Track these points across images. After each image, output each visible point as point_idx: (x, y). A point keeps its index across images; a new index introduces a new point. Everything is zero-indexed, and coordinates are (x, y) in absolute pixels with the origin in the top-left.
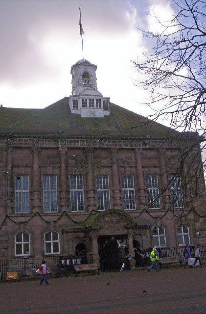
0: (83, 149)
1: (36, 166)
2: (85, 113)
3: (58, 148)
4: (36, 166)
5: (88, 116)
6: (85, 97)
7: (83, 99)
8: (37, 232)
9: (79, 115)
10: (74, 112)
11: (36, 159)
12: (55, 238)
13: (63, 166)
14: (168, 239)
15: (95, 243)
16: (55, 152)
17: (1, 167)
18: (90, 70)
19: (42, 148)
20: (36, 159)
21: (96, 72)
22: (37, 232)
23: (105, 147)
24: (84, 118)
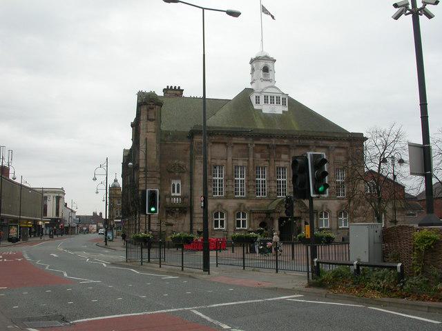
0: (268, 145)
1: (230, 159)
2: (267, 109)
3: (247, 144)
4: (230, 159)
5: (227, 126)
6: (266, 94)
7: (265, 96)
8: (231, 211)
9: (261, 110)
10: (256, 107)
11: (230, 153)
12: (244, 217)
13: (251, 159)
14: (331, 222)
15: (276, 223)
16: (244, 147)
17: (440, 281)
18: (269, 64)
19: (235, 144)
20: (230, 153)
21: (231, 96)
22: (231, 211)
23: (285, 144)
24: (265, 114)
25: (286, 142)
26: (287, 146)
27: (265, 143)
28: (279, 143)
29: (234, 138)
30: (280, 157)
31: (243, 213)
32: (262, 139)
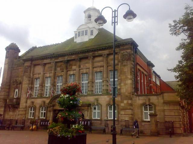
8: (38, 106)
23: (73, 58)
25: (73, 57)
26: (74, 60)
28: (69, 59)
29: (45, 60)
30: (71, 68)
31: (45, 108)
32: (60, 58)
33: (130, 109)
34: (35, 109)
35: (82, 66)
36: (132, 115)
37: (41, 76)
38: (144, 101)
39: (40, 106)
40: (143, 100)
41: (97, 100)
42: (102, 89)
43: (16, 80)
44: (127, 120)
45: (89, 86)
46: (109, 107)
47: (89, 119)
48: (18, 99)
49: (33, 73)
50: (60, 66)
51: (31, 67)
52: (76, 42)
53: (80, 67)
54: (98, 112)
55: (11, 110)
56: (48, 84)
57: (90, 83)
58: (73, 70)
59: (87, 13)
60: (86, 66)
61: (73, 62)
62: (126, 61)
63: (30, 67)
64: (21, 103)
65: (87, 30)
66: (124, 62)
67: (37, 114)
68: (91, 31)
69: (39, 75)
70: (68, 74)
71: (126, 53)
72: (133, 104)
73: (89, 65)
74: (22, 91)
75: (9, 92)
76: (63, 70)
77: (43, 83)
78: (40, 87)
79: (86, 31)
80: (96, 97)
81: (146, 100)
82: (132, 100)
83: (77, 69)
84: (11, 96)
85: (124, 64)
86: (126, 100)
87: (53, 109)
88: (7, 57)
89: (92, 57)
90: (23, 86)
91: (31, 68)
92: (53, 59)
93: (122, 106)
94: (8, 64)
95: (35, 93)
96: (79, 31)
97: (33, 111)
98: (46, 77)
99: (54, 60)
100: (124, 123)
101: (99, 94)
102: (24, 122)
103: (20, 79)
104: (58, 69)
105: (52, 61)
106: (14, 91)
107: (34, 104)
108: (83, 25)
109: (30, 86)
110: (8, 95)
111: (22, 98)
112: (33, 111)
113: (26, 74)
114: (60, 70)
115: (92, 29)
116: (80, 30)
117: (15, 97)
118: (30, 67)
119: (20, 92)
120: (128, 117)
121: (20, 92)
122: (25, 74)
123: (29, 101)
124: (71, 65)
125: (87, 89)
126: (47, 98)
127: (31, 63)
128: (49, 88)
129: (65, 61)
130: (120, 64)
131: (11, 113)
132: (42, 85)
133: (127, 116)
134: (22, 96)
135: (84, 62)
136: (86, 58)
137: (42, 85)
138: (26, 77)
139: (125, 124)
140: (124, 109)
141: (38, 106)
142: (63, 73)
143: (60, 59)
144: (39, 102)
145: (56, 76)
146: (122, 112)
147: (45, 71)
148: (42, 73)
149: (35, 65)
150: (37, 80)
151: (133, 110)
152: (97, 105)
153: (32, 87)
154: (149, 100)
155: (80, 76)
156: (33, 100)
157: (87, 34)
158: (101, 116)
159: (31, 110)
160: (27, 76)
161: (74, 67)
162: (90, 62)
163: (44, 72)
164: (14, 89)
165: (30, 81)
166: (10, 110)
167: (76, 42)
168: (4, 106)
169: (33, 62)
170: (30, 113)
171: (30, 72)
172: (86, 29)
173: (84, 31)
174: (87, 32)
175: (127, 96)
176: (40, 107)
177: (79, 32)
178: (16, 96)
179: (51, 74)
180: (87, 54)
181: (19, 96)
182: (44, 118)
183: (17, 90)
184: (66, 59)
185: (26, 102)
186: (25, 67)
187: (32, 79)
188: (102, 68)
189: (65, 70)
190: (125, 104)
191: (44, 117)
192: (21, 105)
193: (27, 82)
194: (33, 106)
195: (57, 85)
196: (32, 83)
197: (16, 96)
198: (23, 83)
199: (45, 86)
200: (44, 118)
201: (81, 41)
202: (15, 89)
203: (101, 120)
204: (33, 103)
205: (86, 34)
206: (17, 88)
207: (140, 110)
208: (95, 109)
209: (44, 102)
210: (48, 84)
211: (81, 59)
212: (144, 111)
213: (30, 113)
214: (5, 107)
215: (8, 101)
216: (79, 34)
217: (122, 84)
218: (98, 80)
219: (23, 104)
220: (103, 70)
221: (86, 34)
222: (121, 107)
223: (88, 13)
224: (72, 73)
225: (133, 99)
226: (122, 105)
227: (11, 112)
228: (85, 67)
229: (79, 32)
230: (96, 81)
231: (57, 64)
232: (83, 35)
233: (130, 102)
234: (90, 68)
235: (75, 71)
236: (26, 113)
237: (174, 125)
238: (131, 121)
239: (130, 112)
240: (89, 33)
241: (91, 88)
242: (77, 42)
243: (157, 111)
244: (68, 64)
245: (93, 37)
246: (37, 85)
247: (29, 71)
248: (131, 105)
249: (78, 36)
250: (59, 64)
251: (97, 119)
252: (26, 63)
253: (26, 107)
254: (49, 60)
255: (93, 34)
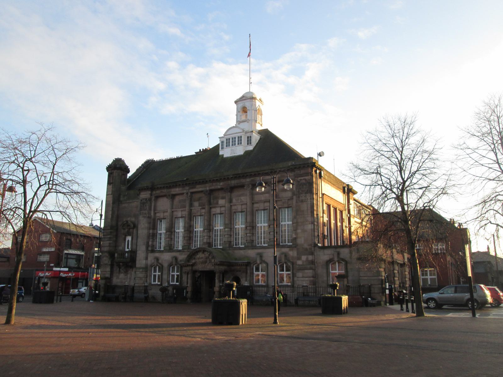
8: (166, 265)
27: (200, 189)
28: (213, 188)
30: (217, 203)
32: (198, 186)
33: (311, 269)
34: (161, 269)
35: (234, 201)
36: (313, 277)
37: (167, 214)
38: (331, 257)
39: (170, 265)
40: (330, 255)
41: (261, 255)
42: (223, 241)
43: (127, 221)
44: (305, 285)
45: (204, 236)
46: (172, 268)
47: (249, 285)
48: (133, 253)
49: (155, 210)
50: (199, 199)
51: (151, 200)
52: (223, 155)
53: (231, 201)
54: (158, 275)
55: (121, 270)
56: (180, 229)
57: (248, 228)
58: (221, 207)
59: (241, 104)
60: (241, 199)
61: (221, 194)
62: (304, 195)
63: (150, 200)
64: (138, 259)
65: (241, 137)
66: (302, 195)
67: (165, 277)
68: (248, 137)
69: (165, 214)
70: (212, 213)
71: (304, 181)
72: (315, 261)
73: (246, 199)
74: (139, 240)
75: (116, 241)
76: (204, 207)
77: (172, 228)
78: (168, 233)
79: (240, 138)
80: (260, 251)
81: (333, 255)
82: (314, 255)
83: (227, 205)
84: (121, 248)
85: (301, 198)
86: (305, 255)
87: (192, 269)
88: (143, 165)
89: (250, 186)
90: (140, 232)
91: (151, 203)
92: (187, 188)
93: (299, 265)
94: (112, 194)
95: (162, 243)
96: (228, 137)
97: (177, 272)
98: (175, 218)
99: (189, 189)
100: (301, 290)
101: (263, 246)
102: (146, 289)
103: (133, 219)
104: (196, 204)
105: (185, 191)
106: (125, 240)
107: (160, 261)
108: (233, 127)
109: (151, 231)
110: (116, 246)
111: (138, 252)
112: (177, 272)
113: (144, 211)
114: (199, 206)
115: (249, 135)
116: (229, 136)
117: (127, 250)
118: (150, 200)
119: (134, 241)
120: (307, 280)
121: (134, 241)
122: (142, 212)
123: (151, 257)
124: (217, 198)
125: (222, 239)
126: (179, 251)
127: (151, 195)
128: (181, 235)
129: (207, 191)
130: (295, 197)
131: (122, 276)
132: (171, 230)
133: (307, 279)
134: (138, 247)
135: (236, 193)
136: (242, 186)
137: (171, 230)
138: (144, 217)
139: (302, 292)
140: (302, 268)
141: (166, 265)
142: (203, 211)
143: (199, 188)
144: (166, 257)
145: (192, 216)
146: (300, 274)
147: (174, 207)
148: (169, 211)
149: (157, 197)
150: (161, 221)
151: (315, 270)
152: (338, 261)
153: (154, 234)
154: (339, 254)
155: (232, 217)
156: (157, 255)
157: (241, 143)
158: (268, 280)
159: (155, 271)
160: (145, 216)
161: (221, 202)
162: (248, 194)
163: (172, 208)
164: (124, 236)
165: (150, 223)
166: (119, 271)
167: (223, 155)
168: (110, 263)
169: (154, 192)
170: (154, 275)
171: (150, 209)
172: (239, 135)
173: (229, 139)
174: (241, 140)
175: (306, 249)
176: (170, 266)
177: (228, 140)
178: (128, 248)
179: (184, 213)
180: (243, 181)
181: (134, 247)
182: (178, 284)
183: (129, 238)
184: (208, 189)
185: (147, 258)
186: (141, 200)
187: (154, 220)
188: (267, 204)
189: (207, 207)
190: (303, 262)
191: (177, 282)
192: (137, 262)
193: (147, 225)
194: (157, 265)
195: (215, 230)
196: (153, 226)
197: (128, 248)
198: (139, 226)
199: (175, 231)
200: (178, 284)
201: (231, 155)
202: (126, 236)
203: (267, 286)
204: (157, 259)
205: (240, 143)
206: (129, 234)
207: (325, 271)
208: (257, 270)
209: (176, 259)
210: (161, 230)
211: (232, 189)
212: (331, 271)
213: (154, 275)
214: (112, 266)
215: (116, 255)
216: (228, 141)
217: (299, 231)
218: (261, 223)
219: (141, 261)
220: (268, 208)
221: (240, 143)
222: (297, 266)
223: (242, 104)
224: (218, 210)
225: (315, 254)
226: (300, 262)
227: (122, 273)
228: (239, 201)
229: (227, 140)
230: (258, 225)
231: (193, 195)
232: (235, 144)
233: (310, 258)
234: (248, 204)
235: (223, 209)
236: (147, 275)
237: (372, 289)
238: (310, 287)
239: (309, 272)
240: (244, 140)
241: (250, 236)
242: (225, 156)
243: (349, 270)
244: (212, 196)
245: (251, 148)
246: (162, 229)
247: (147, 207)
248: (313, 262)
249: (227, 146)
250: (197, 196)
251: (287, 285)
252: (142, 193)
253: (147, 265)
254: (181, 189)
255: (252, 143)
